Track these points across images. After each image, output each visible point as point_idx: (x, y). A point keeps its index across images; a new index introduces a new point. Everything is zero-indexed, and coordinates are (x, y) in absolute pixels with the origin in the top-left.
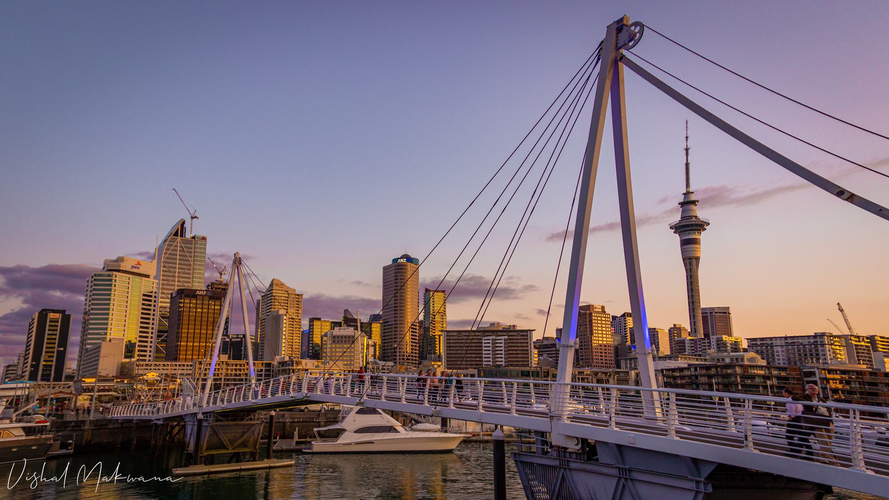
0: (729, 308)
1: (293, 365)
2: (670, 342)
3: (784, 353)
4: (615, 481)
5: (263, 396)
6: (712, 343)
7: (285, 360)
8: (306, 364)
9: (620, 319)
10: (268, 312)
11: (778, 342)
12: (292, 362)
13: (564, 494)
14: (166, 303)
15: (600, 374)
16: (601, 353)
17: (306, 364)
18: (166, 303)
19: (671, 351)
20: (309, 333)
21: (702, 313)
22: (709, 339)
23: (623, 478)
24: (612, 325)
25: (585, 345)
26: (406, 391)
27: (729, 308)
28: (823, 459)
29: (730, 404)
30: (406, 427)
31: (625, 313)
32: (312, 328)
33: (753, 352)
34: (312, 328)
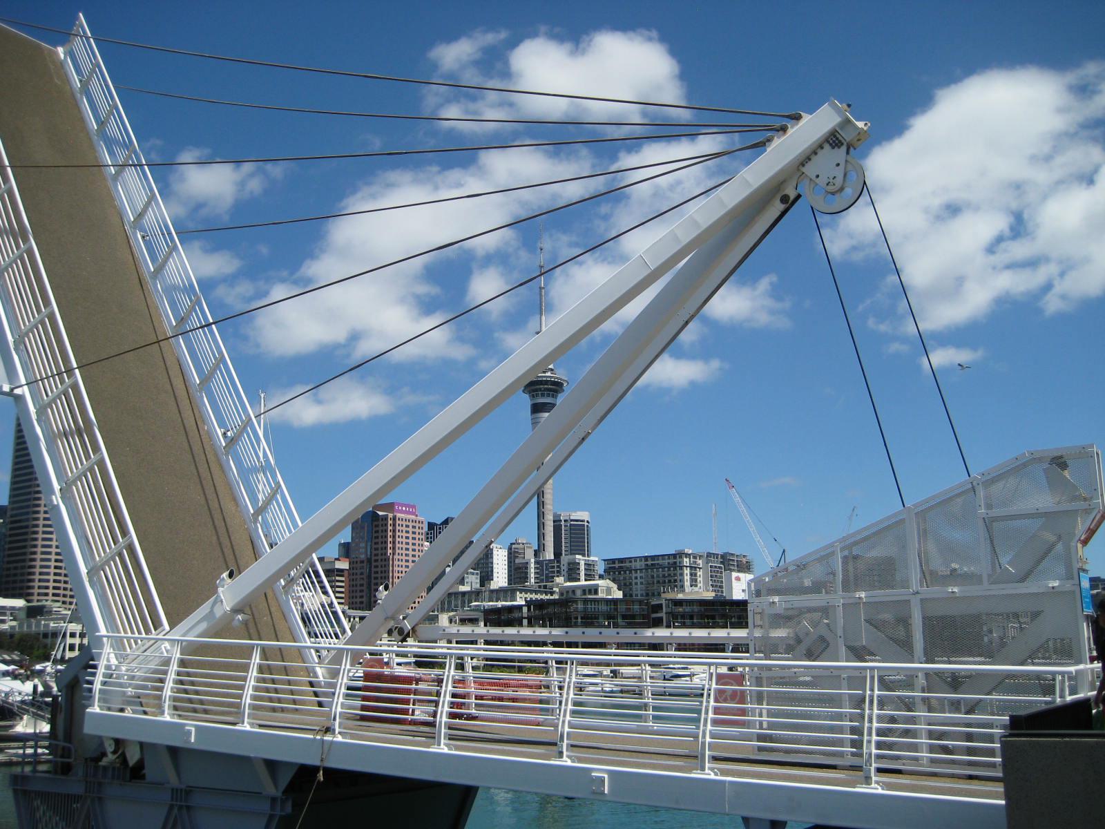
0: (429, 523)
2: (509, 567)
3: (643, 580)
4: (264, 821)
6: (563, 568)
9: (440, 528)
11: (638, 565)
14: (205, 334)
18: (205, 334)
19: (510, 580)
21: (554, 522)
22: (559, 562)
23: (176, 805)
24: (428, 538)
25: (382, 572)
26: (349, 688)
27: (429, 523)
29: (557, 668)
30: (509, 802)
31: (448, 518)
33: (610, 579)
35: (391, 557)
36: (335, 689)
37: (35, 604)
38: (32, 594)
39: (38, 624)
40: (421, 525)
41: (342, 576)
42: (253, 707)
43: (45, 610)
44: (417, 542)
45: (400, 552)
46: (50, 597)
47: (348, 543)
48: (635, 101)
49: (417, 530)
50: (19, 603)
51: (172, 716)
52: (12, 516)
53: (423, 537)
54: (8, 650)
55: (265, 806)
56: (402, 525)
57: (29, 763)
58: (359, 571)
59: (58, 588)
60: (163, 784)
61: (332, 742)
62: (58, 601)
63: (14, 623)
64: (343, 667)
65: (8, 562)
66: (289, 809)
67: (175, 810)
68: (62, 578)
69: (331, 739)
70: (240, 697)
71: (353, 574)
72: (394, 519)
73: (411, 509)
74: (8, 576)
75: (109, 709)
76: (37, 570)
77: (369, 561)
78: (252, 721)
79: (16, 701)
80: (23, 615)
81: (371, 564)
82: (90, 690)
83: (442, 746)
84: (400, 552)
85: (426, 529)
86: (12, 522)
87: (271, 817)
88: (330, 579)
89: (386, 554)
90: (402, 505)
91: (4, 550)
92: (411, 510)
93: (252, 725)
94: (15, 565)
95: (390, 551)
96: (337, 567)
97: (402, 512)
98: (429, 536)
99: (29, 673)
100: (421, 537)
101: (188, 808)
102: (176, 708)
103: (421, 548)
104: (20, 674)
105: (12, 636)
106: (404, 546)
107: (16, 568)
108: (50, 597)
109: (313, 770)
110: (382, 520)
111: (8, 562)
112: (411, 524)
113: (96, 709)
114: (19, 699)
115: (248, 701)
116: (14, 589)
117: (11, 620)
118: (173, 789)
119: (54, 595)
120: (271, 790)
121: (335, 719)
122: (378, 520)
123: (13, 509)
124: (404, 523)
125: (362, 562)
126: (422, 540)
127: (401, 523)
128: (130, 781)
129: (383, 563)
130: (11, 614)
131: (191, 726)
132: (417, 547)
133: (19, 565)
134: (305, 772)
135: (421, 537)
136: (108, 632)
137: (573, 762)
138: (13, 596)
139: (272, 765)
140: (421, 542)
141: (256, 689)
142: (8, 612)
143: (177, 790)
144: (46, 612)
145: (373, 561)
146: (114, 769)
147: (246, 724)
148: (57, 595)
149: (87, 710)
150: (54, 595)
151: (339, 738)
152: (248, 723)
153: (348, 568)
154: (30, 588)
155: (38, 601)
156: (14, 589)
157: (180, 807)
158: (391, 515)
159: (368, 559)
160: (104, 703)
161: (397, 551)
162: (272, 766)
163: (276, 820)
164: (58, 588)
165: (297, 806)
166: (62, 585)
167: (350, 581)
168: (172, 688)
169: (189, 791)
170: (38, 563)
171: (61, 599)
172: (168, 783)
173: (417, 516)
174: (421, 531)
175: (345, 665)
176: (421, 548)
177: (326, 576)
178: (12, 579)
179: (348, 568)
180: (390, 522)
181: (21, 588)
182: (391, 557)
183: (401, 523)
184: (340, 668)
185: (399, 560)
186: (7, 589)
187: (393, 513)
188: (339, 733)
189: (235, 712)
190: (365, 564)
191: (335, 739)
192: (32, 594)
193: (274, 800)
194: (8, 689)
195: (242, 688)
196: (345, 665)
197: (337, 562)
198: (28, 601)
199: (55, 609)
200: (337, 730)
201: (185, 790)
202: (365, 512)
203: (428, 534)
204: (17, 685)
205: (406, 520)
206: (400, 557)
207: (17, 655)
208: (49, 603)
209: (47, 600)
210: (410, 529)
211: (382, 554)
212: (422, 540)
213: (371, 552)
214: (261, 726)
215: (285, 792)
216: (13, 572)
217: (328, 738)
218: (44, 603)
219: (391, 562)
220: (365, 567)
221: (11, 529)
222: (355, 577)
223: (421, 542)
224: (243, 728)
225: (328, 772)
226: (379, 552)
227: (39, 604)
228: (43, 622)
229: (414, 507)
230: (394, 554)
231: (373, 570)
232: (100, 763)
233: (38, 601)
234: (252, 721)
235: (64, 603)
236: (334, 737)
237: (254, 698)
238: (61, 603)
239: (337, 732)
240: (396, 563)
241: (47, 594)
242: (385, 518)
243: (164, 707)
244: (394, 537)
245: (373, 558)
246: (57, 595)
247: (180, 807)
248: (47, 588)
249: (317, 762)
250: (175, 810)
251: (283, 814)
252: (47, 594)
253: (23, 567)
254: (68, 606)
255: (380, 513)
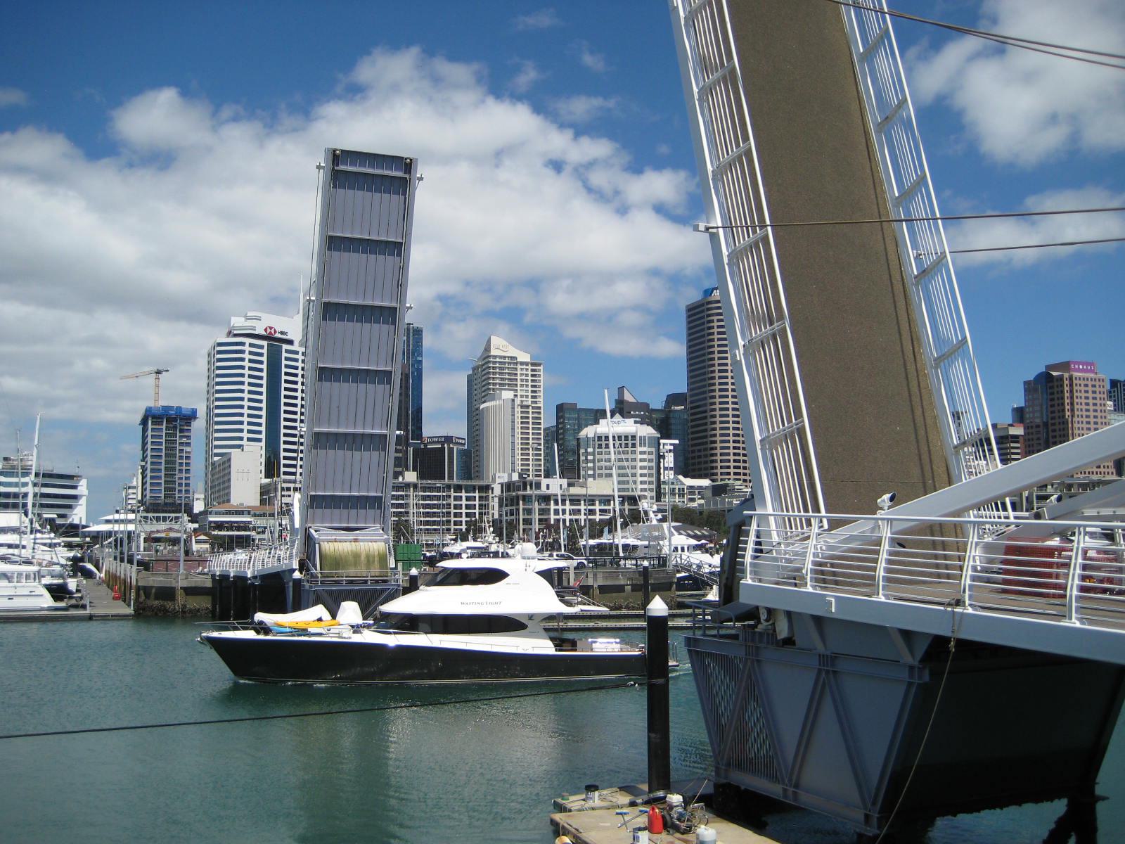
0: (1111, 380)
1: (525, 489)
4: (903, 688)
5: (987, 470)
7: (513, 480)
8: (548, 487)
10: (484, 391)
12: (524, 484)
13: (703, 51)
15: (1076, 486)
16: (1088, 417)
17: (548, 487)
20: (557, 431)
24: (1110, 397)
27: (1111, 380)
28: (1054, 591)
32: (561, 423)
34: (561, 423)
35: (1070, 420)
36: (877, 563)
37: (719, 483)
38: (716, 474)
39: (723, 502)
40: (1101, 383)
41: (1017, 442)
42: (1079, 598)
43: (728, 488)
44: (1098, 402)
45: (1080, 413)
46: (732, 476)
47: (1022, 407)
48: (1119, 54)
49: (1097, 389)
50: (705, 482)
51: (753, 579)
52: (691, 402)
53: (1105, 396)
54: (699, 526)
55: (905, 675)
56: (1080, 385)
57: (700, 628)
58: (1035, 437)
59: (739, 467)
60: (810, 650)
61: (962, 614)
62: (739, 480)
63: (702, 501)
64: (971, 540)
65: (693, 445)
66: (926, 677)
67: (823, 674)
68: (741, 458)
69: (961, 611)
70: (874, 569)
71: (1029, 440)
72: (1071, 378)
73: (1090, 366)
74: (693, 458)
75: (760, 581)
76: (718, 451)
77: (1046, 425)
78: (886, 593)
79: (705, 573)
80: (709, 493)
81: (1047, 428)
82: (743, 563)
83: (1074, 620)
84: (1080, 413)
85: (1108, 386)
86: (692, 408)
87: (910, 684)
88: (1001, 446)
89: (1064, 416)
90: (1079, 363)
91: (688, 434)
92: (1089, 368)
93: (886, 596)
94: (699, 448)
95: (1068, 413)
96: (1011, 433)
97: (1079, 370)
98: (1113, 394)
99: (718, 546)
100: (1102, 396)
101: (835, 672)
102: (817, 580)
103: (1103, 408)
104: (711, 548)
105: (701, 513)
106: (1084, 407)
107: (699, 451)
108: (732, 476)
109: (947, 640)
110: (1057, 380)
111: (693, 445)
112: (1090, 383)
113: (748, 580)
114: (707, 571)
115: (882, 573)
116: (700, 469)
117: (699, 499)
118: (820, 655)
119: (735, 474)
120: (908, 659)
121: (964, 591)
122: (1052, 381)
123: (691, 396)
124: (1083, 383)
125: (1038, 426)
126: (1104, 399)
127: (1078, 382)
128: (782, 646)
129: (1062, 427)
130: (699, 493)
131: (831, 596)
132: (1098, 408)
133: (702, 447)
134: (939, 642)
135: (1102, 396)
136: (774, 511)
137: (1083, 623)
138: (700, 477)
139: (907, 635)
140: (1102, 402)
141: (889, 562)
142: (697, 492)
143: (823, 656)
144: (730, 490)
145: (1050, 425)
146: (768, 634)
147: (880, 595)
148: (738, 474)
149: (741, 582)
150: (735, 474)
151: (970, 610)
152: (1077, 618)
153: (1023, 434)
154: (713, 468)
155: (721, 480)
156: (700, 469)
157: (827, 672)
158: (1066, 375)
159: (1044, 422)
160: (755, 575)
161: (1076, 413)
162: (908, 636)
163: (913, 690)
164: (739, 467)
165: (936, 675)
166: (741, 464)
167: (1026, 447)
168: (885, 568)
169: (834, 658)
170: (718, 445)
171: (742, 477)
172: (815, 649)
173: (1096, 373)
174: (1102, 389)
175: (973, 538)
176: (1103, 408)
177: (997, 443)
178: (697, 460)
179: (1023, 434)
180: (1066, 382)
181: (706, 469)
182: (1070, 420)
183: (1078, 382)
184: (968, 541)
185: (1078, 422)
186: (694, 470)
187: (1069, 372)
188: (970, 605)
189: (869, 582)
190: (1041, 429)
191: (965, 611)
192: (716, 474)
193: (911, 668)
194: (697, 562)
195: (876, 561)
196: (973, 538)
197: (1010, 428)
198: (713, 481)
199: (736, 487)
200: (967, 602)
201: (831, 657)
202: (1036, 373)
203: (1110, 392)
204: (706, 558)
205: (1084, 379)
206: (1080, 419)
207: (706, 530)
208: (731, 482)
209: (729, 479)
210: (1090, 389)
211: (1059, 417)
212: (1104, 399)
213: (1047, 416)
214: (984, 608)
215: (921, 661)
216: (697, 454)
217: (958, 610)
218: (727, 482)
219: (1070, 425)
220: (1042, 432)
221: (692, 414)
222: (1031, 443)
223: (1102, 402)
224: (807, 590)
225: (961, 643)
226: (1056, 415)
227: (723, 482)
228: (727, 500)
229: (1091, 364)
230: (1073, 416)
231: (1051, 434)
232: (756, 630)
233: (721, 480)
234: (886, 593)
235: (745, 481)
236: (964, 609)
237: (887, 570)
238: (741, 482)
239: (967, 604)
240: (1076, 425)
241: (729, 474)
242: (1061, 378)
243: (806, 579)
244: (1072, 398)
245: (1050, 422)
246: (738, 474)
247: (827, 672)
248: (729, 467)
249: (948, 634)
250: (823, 674)
251: (921, 682)
252: (729, 474)
253: (706, 449)
254: (748, 484)
255: (1054, 374)
